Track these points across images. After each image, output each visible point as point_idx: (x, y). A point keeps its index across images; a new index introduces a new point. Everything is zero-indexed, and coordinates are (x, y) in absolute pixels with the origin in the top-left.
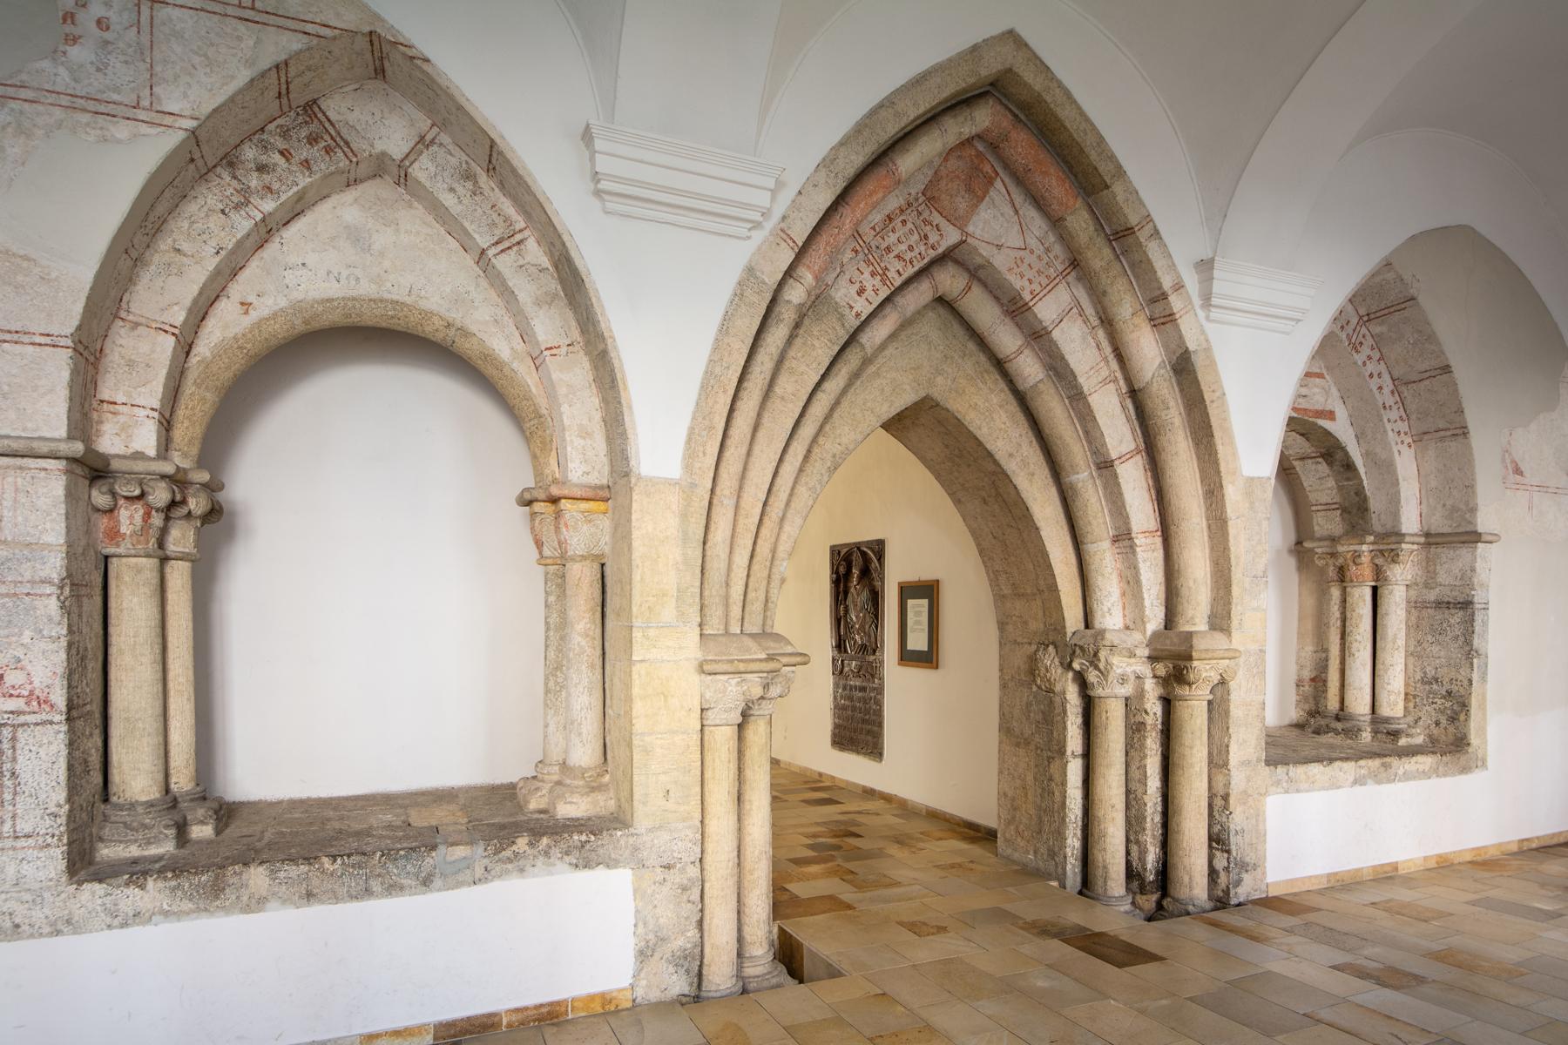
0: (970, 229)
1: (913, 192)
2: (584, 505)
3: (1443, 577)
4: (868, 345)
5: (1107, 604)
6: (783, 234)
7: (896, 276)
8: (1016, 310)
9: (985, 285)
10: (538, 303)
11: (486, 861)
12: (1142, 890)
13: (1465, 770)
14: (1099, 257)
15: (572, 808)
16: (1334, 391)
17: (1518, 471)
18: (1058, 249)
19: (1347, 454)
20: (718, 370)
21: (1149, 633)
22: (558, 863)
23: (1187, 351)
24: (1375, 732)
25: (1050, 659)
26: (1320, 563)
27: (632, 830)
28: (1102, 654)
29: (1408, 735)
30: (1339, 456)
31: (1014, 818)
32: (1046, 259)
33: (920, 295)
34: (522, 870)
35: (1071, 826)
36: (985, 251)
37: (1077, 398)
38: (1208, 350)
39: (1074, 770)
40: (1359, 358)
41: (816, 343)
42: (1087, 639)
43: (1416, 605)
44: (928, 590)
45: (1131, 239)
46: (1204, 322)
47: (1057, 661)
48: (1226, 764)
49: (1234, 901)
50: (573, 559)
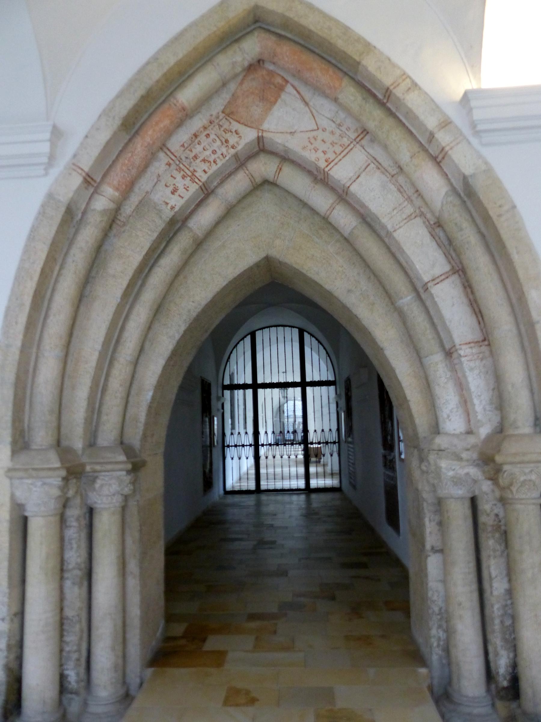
0: (265, 126)
1: (214, 113)
7: (203, 174)
23: (465, 179)
28: (432, 457)
32: (338, 132)
38: (489, 171)
41: (139, 233)
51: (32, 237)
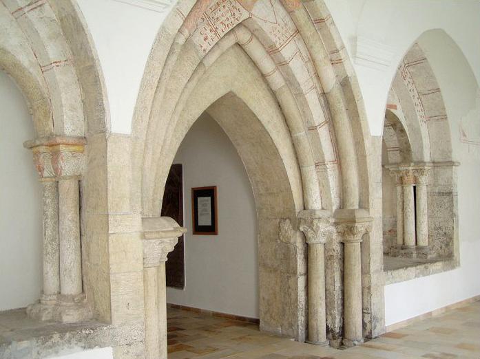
0: (253, 12)
2: (72, 148)
3: (441, 182)
4: (206, 65)
5: (315, 197)
6: (178, 11)
8: (272, 51)
9: (257, 38)
10: (50, 38)
11: (38, 348)
12: (334, 338)
13: (453, 267)
14: (309, 30)
15: (70, 317)
16: (396, 97)
17: (465, 135)
18: (290, 24)
19: (402, 126)
20: (148, 78)
21: (334, 211)
22: (76, 347)
24: (418, 253)
25: (287, 226)
26: (391, 175)
27: (112, 326)
28: (315, 222)
29: (430, 254)
30: (398, 125)
31: (269, 309)
33: (231, 41)
34: (57, 352)
35: (300, 310)
36: (260, 23)
37: (299, 94)
39: (301, 281)
40: (406, 82)
42: (306, 214)
43: (430, 194)
44: (210, 192)
45: (322, 24)
46: (352, 63)
47: (291, 227)
48: (369, 272)
49: (374, 336)
50: (65, 178)
51: (152, 57)
